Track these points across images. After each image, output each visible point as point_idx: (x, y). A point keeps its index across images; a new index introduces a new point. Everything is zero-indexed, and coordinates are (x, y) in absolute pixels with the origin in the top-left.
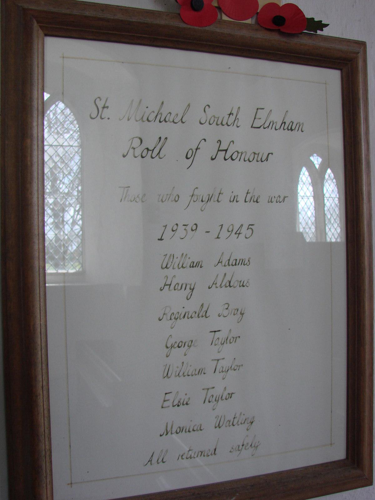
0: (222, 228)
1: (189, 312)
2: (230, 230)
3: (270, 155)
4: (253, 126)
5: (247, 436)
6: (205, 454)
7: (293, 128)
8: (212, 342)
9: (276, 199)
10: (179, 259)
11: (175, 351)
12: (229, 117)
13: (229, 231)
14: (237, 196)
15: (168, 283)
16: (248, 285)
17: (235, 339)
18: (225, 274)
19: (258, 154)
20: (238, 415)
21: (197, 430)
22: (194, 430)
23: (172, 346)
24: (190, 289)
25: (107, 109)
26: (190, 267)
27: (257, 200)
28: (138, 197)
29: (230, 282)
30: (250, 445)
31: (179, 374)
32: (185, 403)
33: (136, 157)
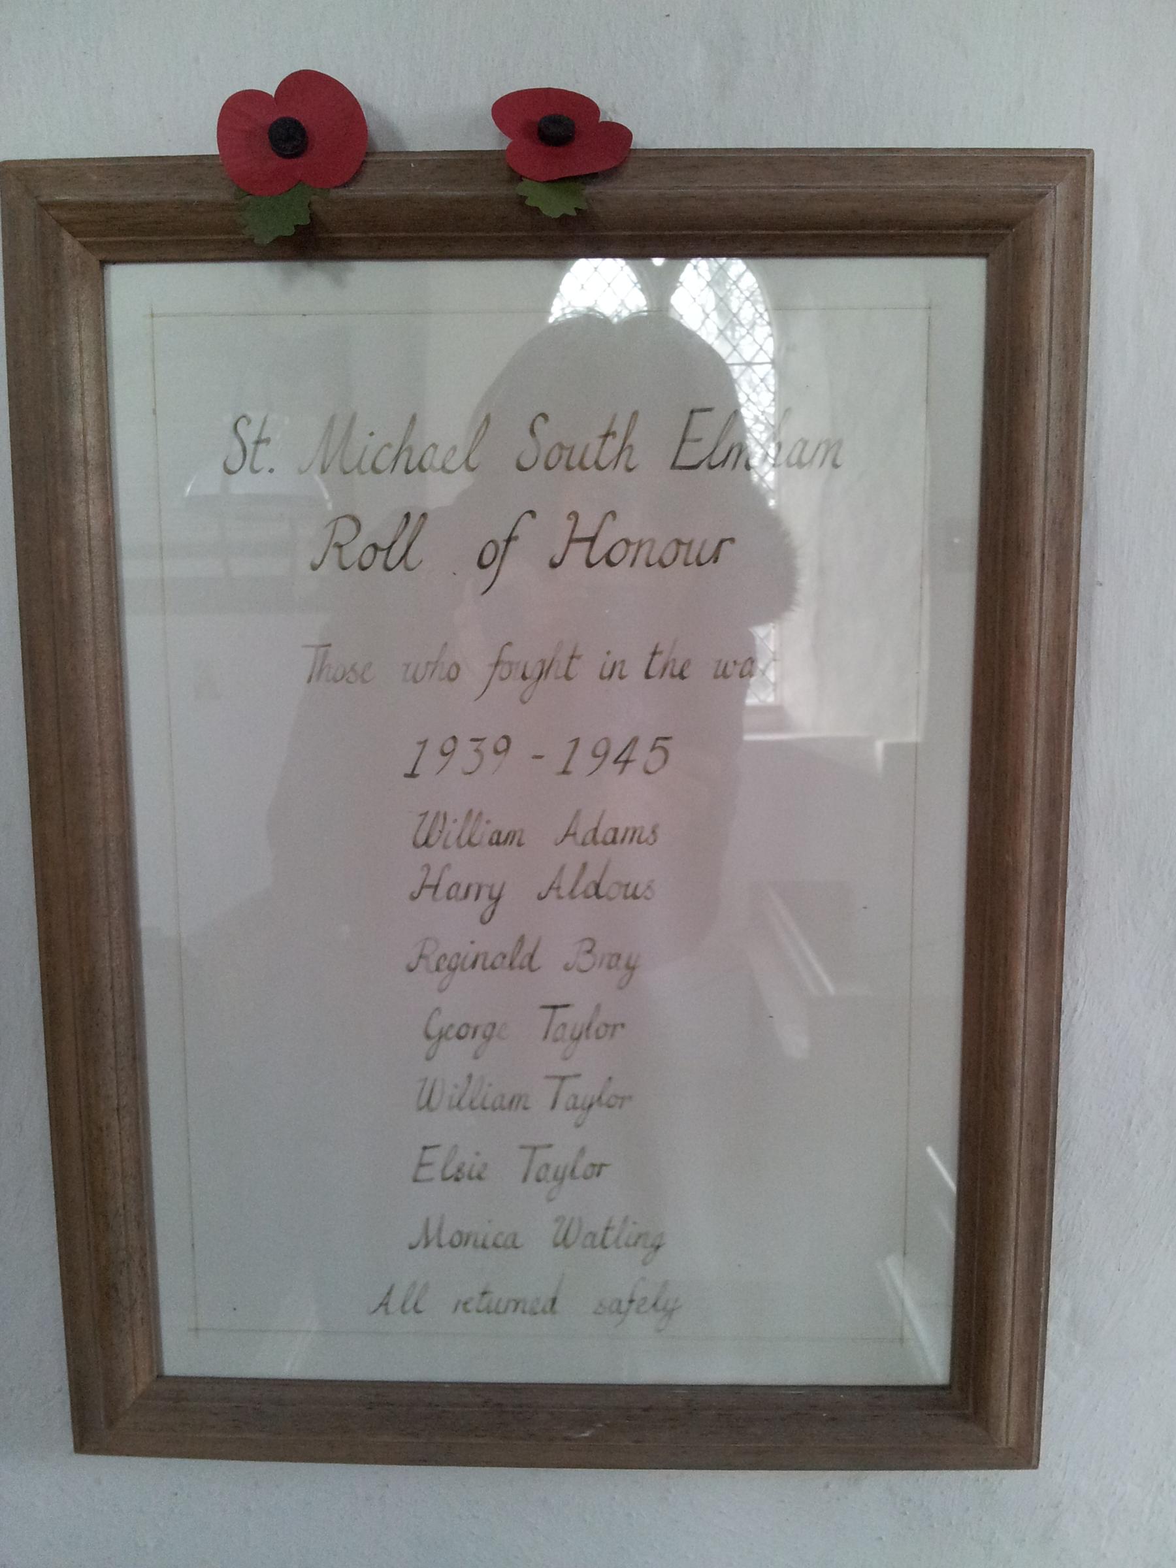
0: (576, 746)
1: (486, 954)
2: (601, 751)
3: (726, 544)
4: (678, 463)
5: (643, 1279)
6: (527, 1309)
7: (805, 459)
8: (547, 1032)
9: (738, 668)
10: (461, 822)
11: (450, 1047)
12: (603, 444)
13: (595, 756)
14: (623, 662)
15: (432, 881)
16: (648, 894)
17: (613, 1028)
18: (585, 865)
19: (690, 544)
20: (616, 1223)
21: (505, 1246)
22: (495, 1245)
23: (442, 1035)
24: (490, 897)
25: (267, 445)
26: (491, 843)
27: (682, 671)
28: (352, 669)
29: (597, 886)
30: (651, 1301)
31: (459, 1103)
32: (474, 1174)
33: (344, 569)
